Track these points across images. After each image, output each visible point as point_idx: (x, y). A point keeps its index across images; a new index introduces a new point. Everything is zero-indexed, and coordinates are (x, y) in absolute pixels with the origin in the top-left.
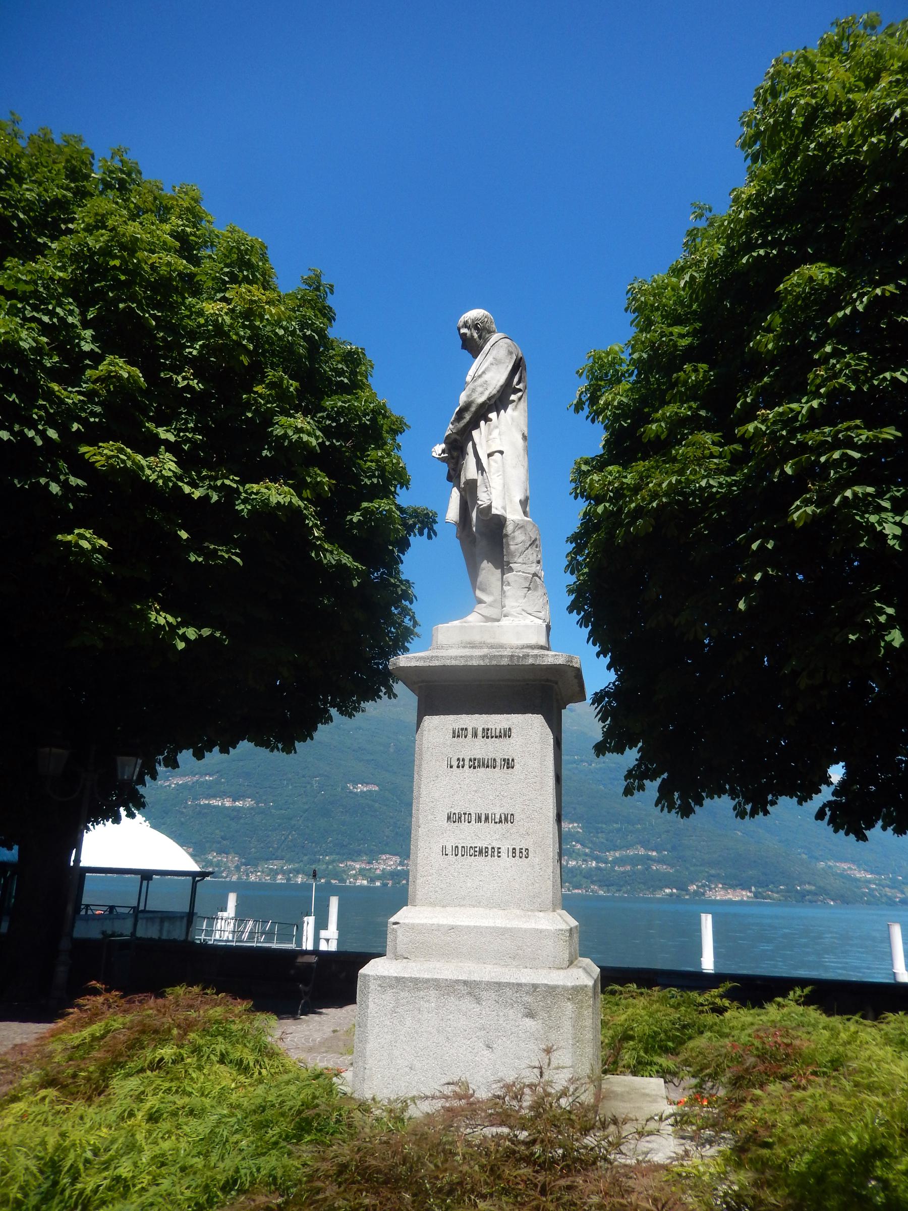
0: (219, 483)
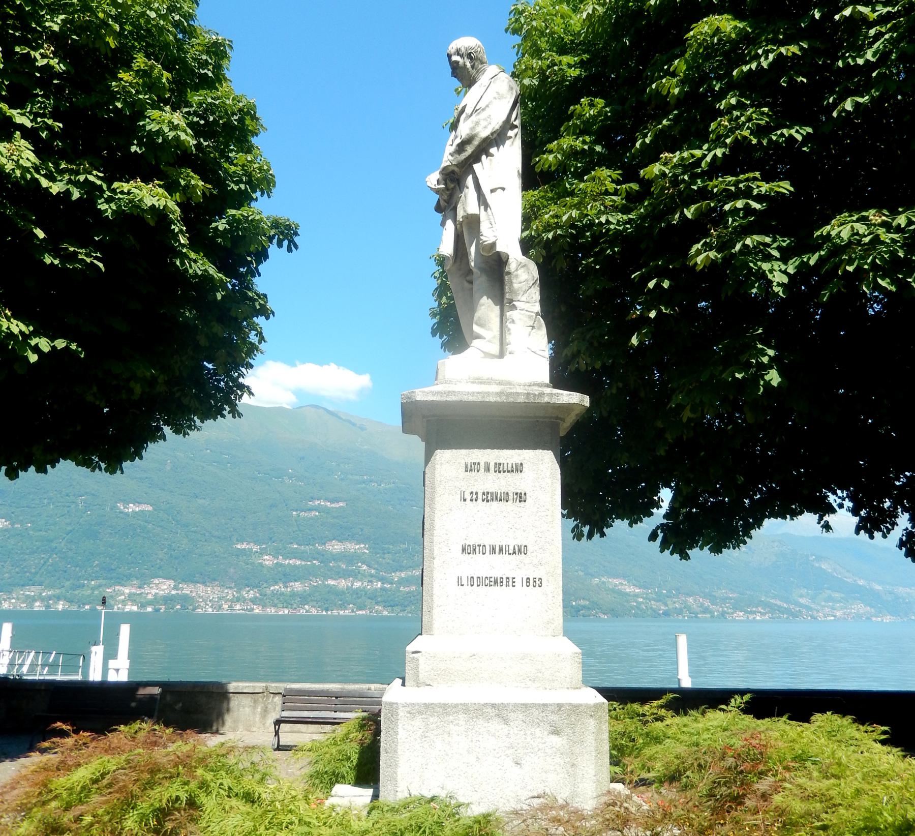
0: (82, 178)
